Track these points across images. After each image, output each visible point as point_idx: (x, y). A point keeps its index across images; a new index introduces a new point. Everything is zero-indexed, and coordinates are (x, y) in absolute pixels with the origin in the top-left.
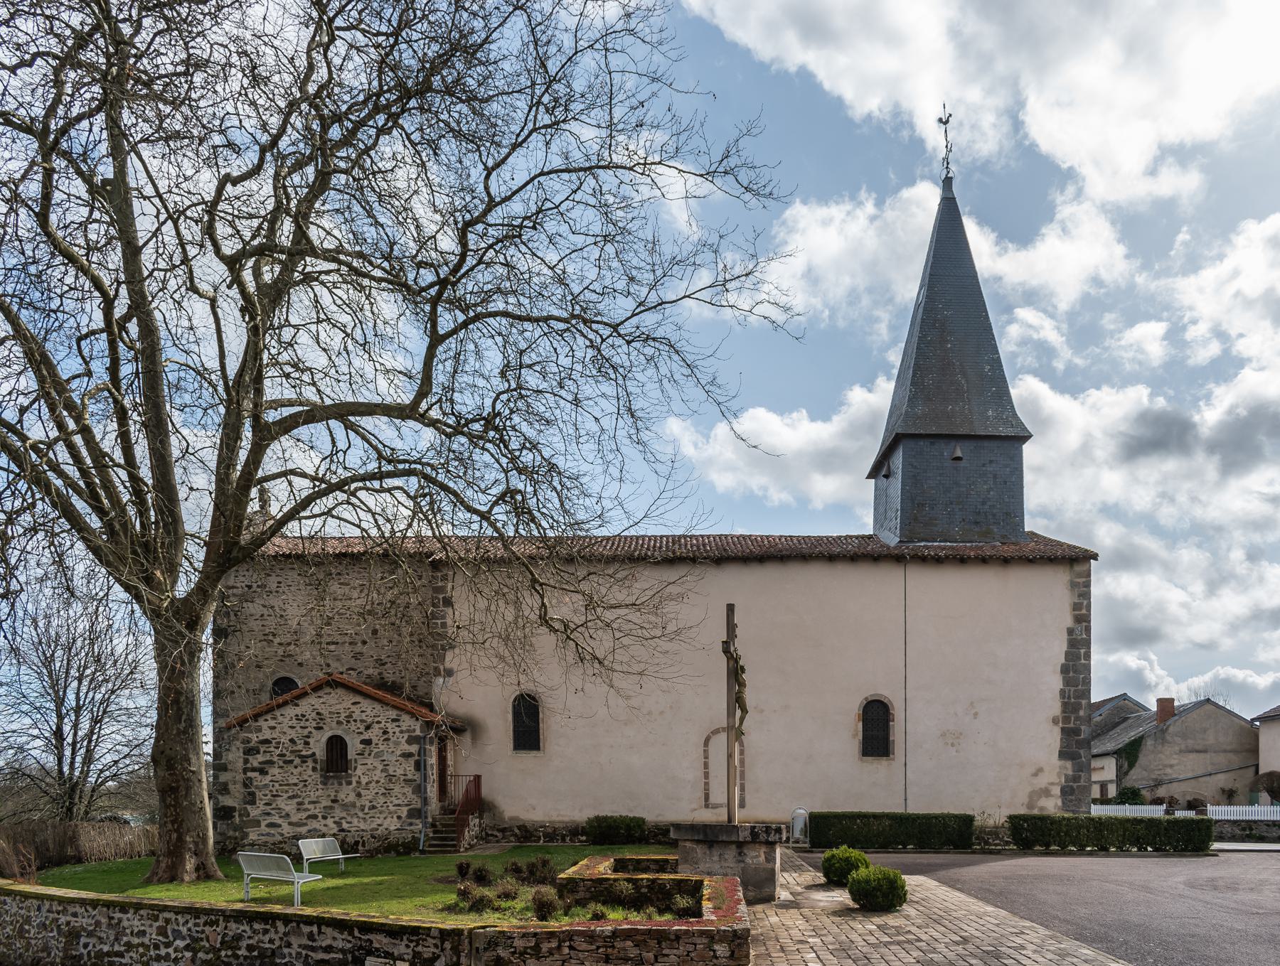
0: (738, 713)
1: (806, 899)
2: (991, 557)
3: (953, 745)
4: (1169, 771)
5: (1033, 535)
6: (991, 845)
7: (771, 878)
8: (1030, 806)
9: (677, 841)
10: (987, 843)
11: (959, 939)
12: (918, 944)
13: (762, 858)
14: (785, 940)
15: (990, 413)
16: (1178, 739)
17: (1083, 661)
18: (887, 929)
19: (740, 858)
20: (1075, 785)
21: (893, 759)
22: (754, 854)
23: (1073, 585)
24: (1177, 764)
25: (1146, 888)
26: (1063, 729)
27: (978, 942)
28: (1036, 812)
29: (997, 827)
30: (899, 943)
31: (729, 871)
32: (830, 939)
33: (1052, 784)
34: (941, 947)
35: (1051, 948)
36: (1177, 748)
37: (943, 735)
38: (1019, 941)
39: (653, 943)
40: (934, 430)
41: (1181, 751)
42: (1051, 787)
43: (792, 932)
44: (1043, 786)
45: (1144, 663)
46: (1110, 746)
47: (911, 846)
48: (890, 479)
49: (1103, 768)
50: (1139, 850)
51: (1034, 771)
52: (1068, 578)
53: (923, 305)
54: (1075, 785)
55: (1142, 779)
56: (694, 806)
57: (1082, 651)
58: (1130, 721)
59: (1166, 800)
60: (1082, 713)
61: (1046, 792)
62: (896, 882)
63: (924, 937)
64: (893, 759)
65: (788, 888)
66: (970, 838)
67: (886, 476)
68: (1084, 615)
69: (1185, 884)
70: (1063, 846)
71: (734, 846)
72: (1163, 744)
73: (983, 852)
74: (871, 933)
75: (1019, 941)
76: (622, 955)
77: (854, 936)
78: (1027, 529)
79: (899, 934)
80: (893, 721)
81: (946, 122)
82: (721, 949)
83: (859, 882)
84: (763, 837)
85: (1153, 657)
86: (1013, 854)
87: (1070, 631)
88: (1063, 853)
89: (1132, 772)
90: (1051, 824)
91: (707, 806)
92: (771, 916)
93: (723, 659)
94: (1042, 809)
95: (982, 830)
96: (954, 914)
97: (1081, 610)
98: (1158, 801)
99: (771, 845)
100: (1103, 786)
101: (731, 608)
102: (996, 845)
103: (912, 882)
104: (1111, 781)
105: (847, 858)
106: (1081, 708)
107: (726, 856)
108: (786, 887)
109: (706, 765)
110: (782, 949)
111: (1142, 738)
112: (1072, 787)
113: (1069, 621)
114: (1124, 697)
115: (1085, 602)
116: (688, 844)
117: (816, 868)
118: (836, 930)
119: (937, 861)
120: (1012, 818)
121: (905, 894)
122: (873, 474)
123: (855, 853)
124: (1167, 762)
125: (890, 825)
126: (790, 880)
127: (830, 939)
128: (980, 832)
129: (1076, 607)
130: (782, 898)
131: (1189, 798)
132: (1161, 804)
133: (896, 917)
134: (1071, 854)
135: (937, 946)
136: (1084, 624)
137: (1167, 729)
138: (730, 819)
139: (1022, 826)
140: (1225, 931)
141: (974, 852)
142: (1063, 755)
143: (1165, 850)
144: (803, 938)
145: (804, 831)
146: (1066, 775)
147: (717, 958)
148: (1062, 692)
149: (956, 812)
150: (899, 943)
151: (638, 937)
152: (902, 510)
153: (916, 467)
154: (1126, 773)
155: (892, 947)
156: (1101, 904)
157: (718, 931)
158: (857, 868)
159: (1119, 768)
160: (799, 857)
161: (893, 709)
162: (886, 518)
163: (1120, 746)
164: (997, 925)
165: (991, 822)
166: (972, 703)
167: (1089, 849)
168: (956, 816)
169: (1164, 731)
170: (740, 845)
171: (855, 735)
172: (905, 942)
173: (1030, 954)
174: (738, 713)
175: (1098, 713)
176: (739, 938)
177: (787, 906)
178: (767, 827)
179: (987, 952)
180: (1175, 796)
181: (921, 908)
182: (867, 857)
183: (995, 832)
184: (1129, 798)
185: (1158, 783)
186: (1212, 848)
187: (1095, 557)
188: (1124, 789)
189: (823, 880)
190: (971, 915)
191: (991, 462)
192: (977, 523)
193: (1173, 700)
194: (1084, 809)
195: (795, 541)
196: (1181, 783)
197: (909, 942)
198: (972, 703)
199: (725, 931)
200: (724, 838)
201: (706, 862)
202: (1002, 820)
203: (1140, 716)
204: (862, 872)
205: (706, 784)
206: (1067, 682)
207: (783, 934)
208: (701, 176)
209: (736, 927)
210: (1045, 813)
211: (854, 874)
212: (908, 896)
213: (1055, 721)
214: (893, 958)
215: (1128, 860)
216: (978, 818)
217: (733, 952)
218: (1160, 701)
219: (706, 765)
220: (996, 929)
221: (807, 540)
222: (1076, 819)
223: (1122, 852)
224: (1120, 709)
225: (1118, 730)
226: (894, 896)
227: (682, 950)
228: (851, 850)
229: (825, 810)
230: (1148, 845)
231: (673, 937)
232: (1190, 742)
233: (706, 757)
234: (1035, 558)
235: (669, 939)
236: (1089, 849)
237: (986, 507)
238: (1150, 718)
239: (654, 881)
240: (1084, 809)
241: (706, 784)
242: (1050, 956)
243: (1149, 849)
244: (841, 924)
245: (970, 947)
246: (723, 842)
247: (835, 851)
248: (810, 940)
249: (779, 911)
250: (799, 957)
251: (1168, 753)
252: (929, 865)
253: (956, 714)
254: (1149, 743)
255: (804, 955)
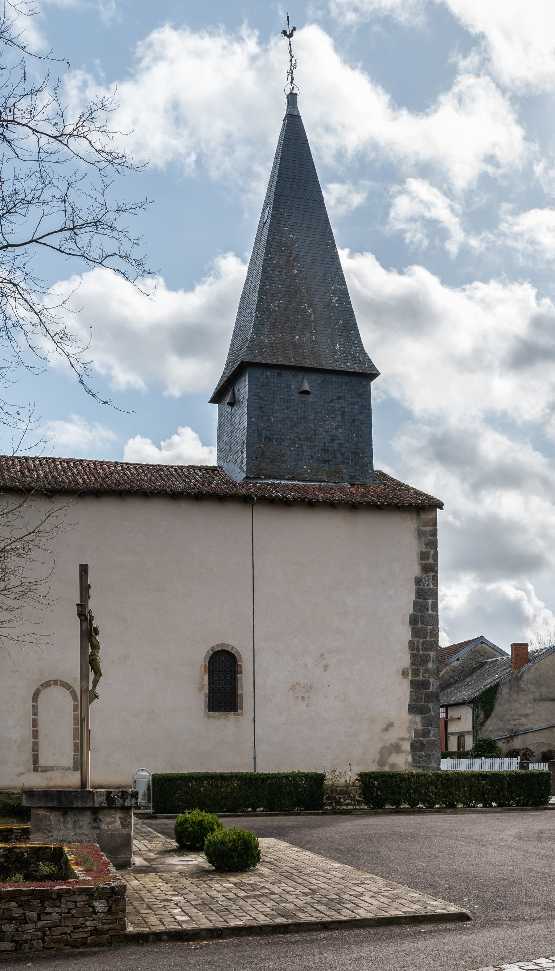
0: (92, 675)
1: (162, 864)
2: (339, 502)
3: (303, 699)
4: (524, 720)
5: (382, 475)
6: (342, 804)
7: (127, 843)
8: (381, 763)
9: (28, 809)
10: (338, 803)
11: (308, 890)
12: (272, 897)
13: (118, 824)
14: (149, 899)
15: (338, 347)
16: (532, 688)
17: (430, 612)
18: (243, 886)
19: (95, 825)
20: (425, 740)
21: (242, 715)
22: (109, 819)
23: (420, 534)
24: (532, 714)
25: (480, 842)
26: (412, 682)
27: (324, 892)
28: (387, 769)
29: (348, 786)
30: (255, 897)
31: (84, 838)
32: (192, 896)
33: (403, 739)
34: (292, 898)
35: (386, 894)
36: (531, 697)
37: (293, 688)
38: (359, 889)
39: (36, 903)
40: (280, 361)
41: (535, 700)
42: (401, 743)
43: (156, 893)
44: (394, 742)
45: (522, 594)
46: (467, 694)
47: (261, 809)
48: (236, 408)
49: (459, 718)
50: (485, 806)
51: (384, 726)
52: (416, 526)
53: (268, 224)
54: (425, 740)
55: (499, 730)
56: (21, 769)
57: (430, 601)
58: (487, 666)
59: (521, 753)
60: (430, 665)
61: (397, 748)
62: (250, 842)
63: (277, 891)
64: (242, 715)
65: (141, 855)
66: (322, 799)
67: (232, 404)
68: (431, 564)
69: (515, 836)
70: (413, 804)
71: (89, 813)
72: (518, 693)
73: (335, 812)
74: (229, 890)
75: (359, 889)
76: (6, 915)
77: (213, 893)
78: (375, 469)
79: (254, 889)
80: (241, 673)
81: (290, 36)
82: (100, 905)
83: (215, 843)
84: (119, 802)
85: (530, 586)
86: (365, 813)
87: (418, 581)
88: (413, 810)
89: (488, 722)
90: (401, 781)
91: (36, 769)
92: (131, 880)
93: (77, 621)
94: (393, 765)
95: (334, 789)
96: (304, 871)
97: (428, 559)
98: (513, 754)
99: (126, 809)
100: (460, 737)
101: (84, 569)
102: (347, 805)
103: (264, 843)
104: (468, 733)
105: (201, 821)
106: (429, 660)
107: (81, 823)
108: (139, 853)
109: (35, 723)
110: (149, 907)
111: (497, 686)
112: (421, 742)
113: (416, 571)
114: (481, 640)
115: (432, 551)
116: (41, 812)
117: (166, 834)
118: (196, 889)
119: (288, 823)
120: (363, 776)
121: (258, 854)
122: (217, 398)
123: (207, 817)
124: (522, 712)
125: (239, 787)
126: (141, 846)
127: (192, 896)
128: (331, 792)
129: (423, 556)
130: (137, 864)
131: (545, 749)
132: (516, 757)
133: (251, 876)
134: (420, 812)
135: (289, 897)
136: (431, 574)
137: (521, 676)
138: (83, 784)
139: (372, 784)
140: (534, 874)
141: (325, 813)
142: (413, 709)
143: (511, 806)
144: (166, 897)
145: (148, 796)
146: (416, 730)
147: (96, 913)
148: (411, 643)
149: (306, 771)
150: (255, 897)
151: (22, 898)
152: (248, 443)
153: (262, 399)
154: (482, 724)
155: (249, 900)
156: (437, 857)
157: (97, 889)
158: (212, 830)
159: (475, 719)
160: (144, 824)
161: (241, 661)
162: (230, 449)
163: (476, 694)
164: (342, 878)
165: (342, 781)
166: (322, 655)
167: (437, 806)
168: (306, 775)
169: (518, 679)
170: (95, 811)
171: (201, 689)
172: (260, 895)
173: (367, 898)
174: (92, 675)
175: (455, 657)
176: (116, 894)
177: (143, 871)
178: (123, 792)
179: (332, 900)
180: (531, 748)
181: (273, 867)
182: (221, 820)
183: (345, 791)
184: (485, 751)
185: (514, 734)
186: (551, 802)
187: (440, 506)
188: (480, 741)
189: (174, 844)
190: (320, 871)
191: (339, 398)
192: (325, 461)
193: (526, 645)
194: (433, 765)
195: (133, 470)
196: (537, 734)
197: (263, 895)
198: (322, 655)
199: (103, 888)
200: (80, 804)
201: (59, 830)
202: (353, 779)
203: (497, 661)
204: (217, 835)
205: (35, 744)
206: (416, 633)
207: (147, 895)
208: (55, 137)
209: (113, 884)
210: (395, 770)
211: (210, 836)
212: (262, 858)
213: (404, 674)
214: (251, 908)
215: (474, 816)
216: (329, 777)
217: (110, 908)
218: (515, 647)
219: (35, 723)
220: (341, 881)
221: (146, 470)
222: (424, 775)
223: (469, 807)
224: (477, 653)
225: (475, 676)
226: (248, 856)
227: (63, 909)
228: (203, 813)
229: (169, 771)
230: (492, 801)
231: (54, 896)
232: (544, 690)
233: (35, 714)
234: (382, 504)
235: (52, 899)
236: (437, 806)
237: (335, 445)
238: (505, 664)
239: (11, 850)
240: (433, 765)
241: (35, 744)
242: (383, 899)
243: (494, 804)
244: (200, 884)
245: (317, 896)
246: (78, 808)
247: (187, 815)
248: (173, 898)
249: (138, 876)
250: (167, 912)
251: (522, 702)
252: (280, 827)
253: (306, 666)
254: (504, 691)
255: (170, 910)
